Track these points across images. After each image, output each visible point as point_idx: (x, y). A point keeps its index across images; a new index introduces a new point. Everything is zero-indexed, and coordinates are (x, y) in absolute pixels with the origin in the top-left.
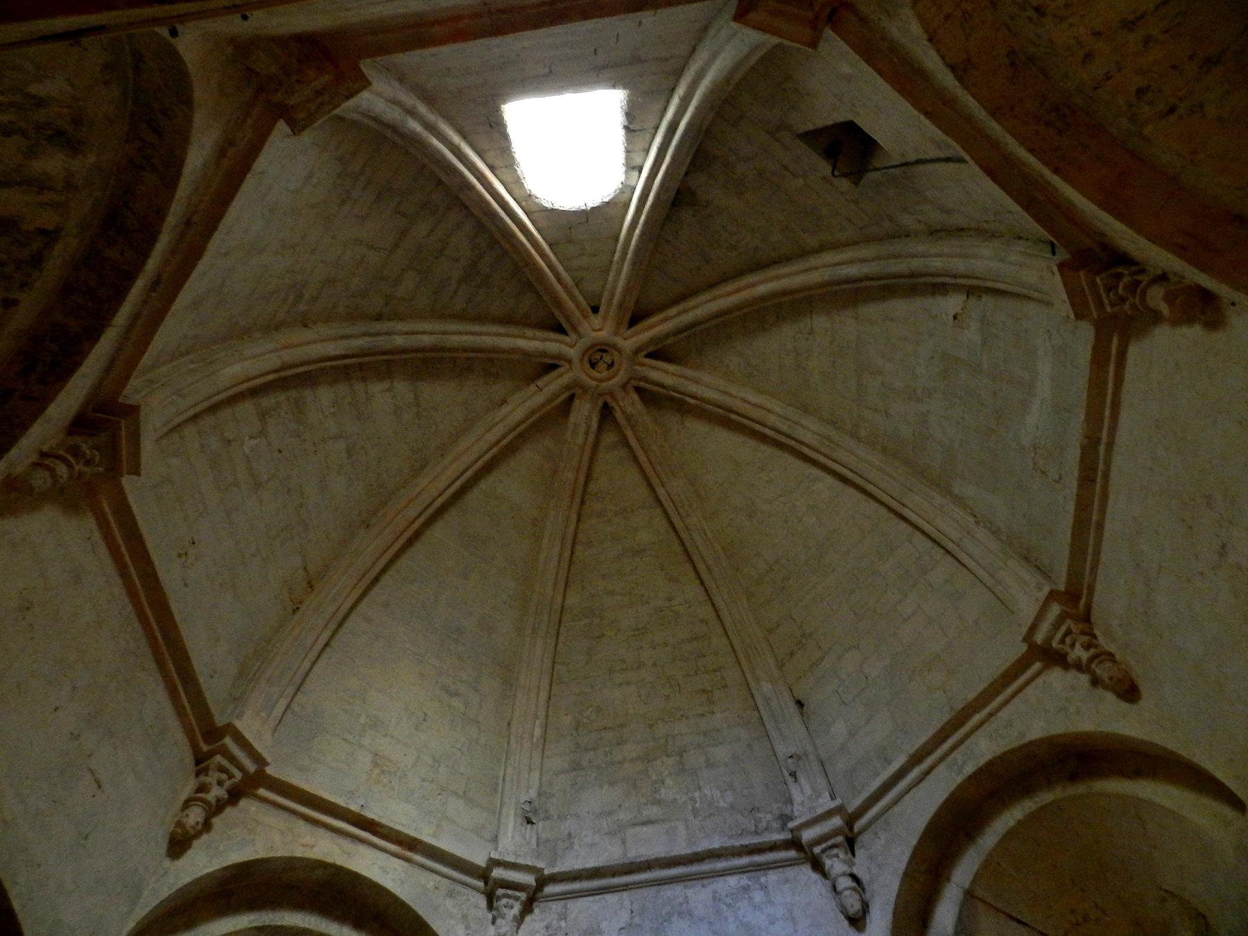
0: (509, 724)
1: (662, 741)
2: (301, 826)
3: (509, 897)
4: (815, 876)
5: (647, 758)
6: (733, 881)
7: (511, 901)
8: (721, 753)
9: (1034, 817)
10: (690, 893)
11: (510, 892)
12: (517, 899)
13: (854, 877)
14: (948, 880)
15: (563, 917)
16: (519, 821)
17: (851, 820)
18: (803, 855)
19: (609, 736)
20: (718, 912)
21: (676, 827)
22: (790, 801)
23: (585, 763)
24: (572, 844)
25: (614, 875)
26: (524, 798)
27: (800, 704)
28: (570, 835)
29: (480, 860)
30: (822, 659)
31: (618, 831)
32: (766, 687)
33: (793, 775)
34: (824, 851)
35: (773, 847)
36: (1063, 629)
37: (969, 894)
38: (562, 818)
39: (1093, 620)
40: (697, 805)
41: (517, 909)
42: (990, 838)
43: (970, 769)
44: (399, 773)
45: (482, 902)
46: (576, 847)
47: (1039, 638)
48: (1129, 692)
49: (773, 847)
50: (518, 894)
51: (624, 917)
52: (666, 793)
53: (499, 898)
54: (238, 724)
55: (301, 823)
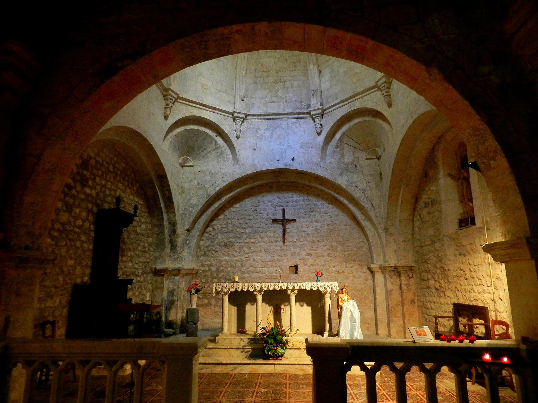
0: (236, 68)
1: (280, 78)
2: (189, 108)
3: (239, 120)
4: (312, 122)
5: (275, 82)
6: (293, 120)
7: (239, 121)
8: (295, 84)
9: (362, 122)
10: (282, 122)
11: (239, 119)
12: (240, 120)
13: (321, 125)
14: (341, 129)
15: (251, 124)
16: (240, 100)
17: (323, 111)
18: (310, 116)
19: (265, 74)
20: (288, 128)
21: (280, 104)
22: (310, 101)
23: (258, 82)
24: (254, 106)
25: (264, 116)
26: (242, 94)
27: (320, 72)
28: (253, 103)
29: (231, 111)
30: (329, 60)
31: (265, 104)
32: (311, 66)
33: (313, 95)
34: (315, 117)
35: (304, 113)
36: (384, 85)
37: (344, 133)
38: (251, 98)
39: (392, 84)
40: (287, 99)
41: (240, 123)
42: (352, 123)
43: (353, 109)
44: (209, 88)
45: (232, 120)
46: (255, 107)
47: (379, 84)
48: (390, 105)
49: (304, 113)
50: (241, 119)
51: (266, 126)
52: (280, 94)
53: (236, 120)
54: (171, 88)
55: (189, 106)
